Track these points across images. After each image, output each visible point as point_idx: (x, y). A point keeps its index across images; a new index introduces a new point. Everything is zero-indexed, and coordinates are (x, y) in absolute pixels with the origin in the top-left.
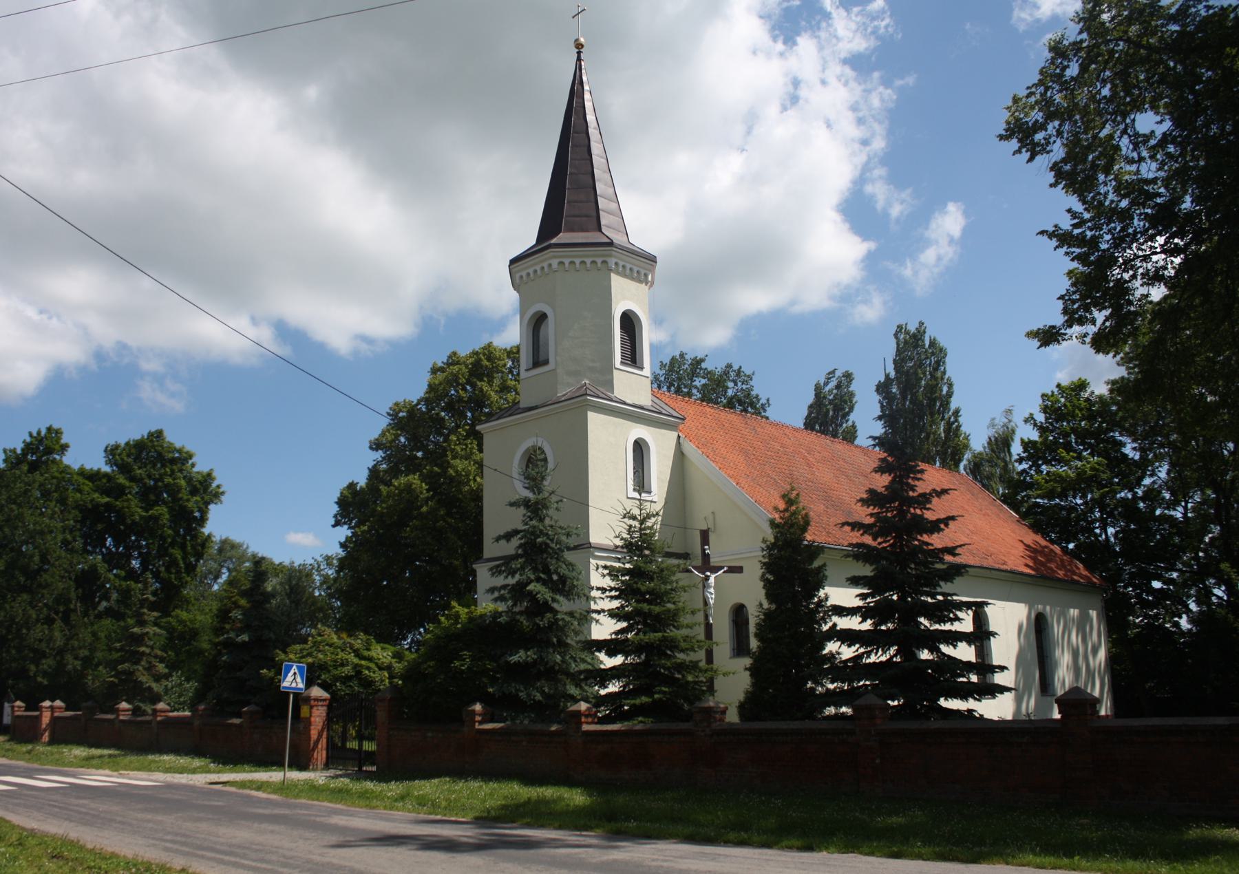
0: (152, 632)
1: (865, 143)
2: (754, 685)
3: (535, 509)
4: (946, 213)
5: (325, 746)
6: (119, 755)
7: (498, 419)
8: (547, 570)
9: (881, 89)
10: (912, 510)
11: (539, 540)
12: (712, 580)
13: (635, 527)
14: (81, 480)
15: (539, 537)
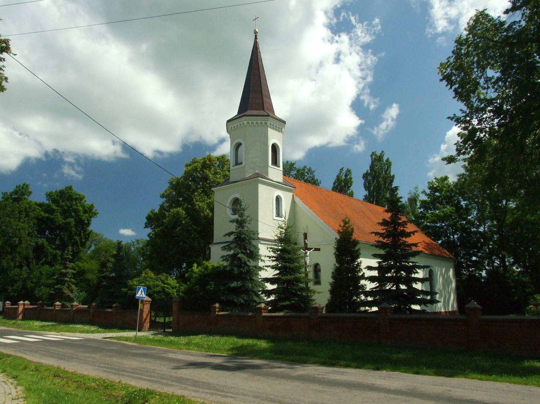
0: (70, 272)
1: (364, 78)
2: (332, 297)
3: (240, 223)
4: (392, 108)
5: (149, 320)
6: (57, 325)
7: (221, 186)
8: (245, 249)
9: (372, 56)
10: (399, 228)
11: (242, 236)
12: (308, 254)
13: (283, 232)
14: (37, 207)
15: (242, 235)
